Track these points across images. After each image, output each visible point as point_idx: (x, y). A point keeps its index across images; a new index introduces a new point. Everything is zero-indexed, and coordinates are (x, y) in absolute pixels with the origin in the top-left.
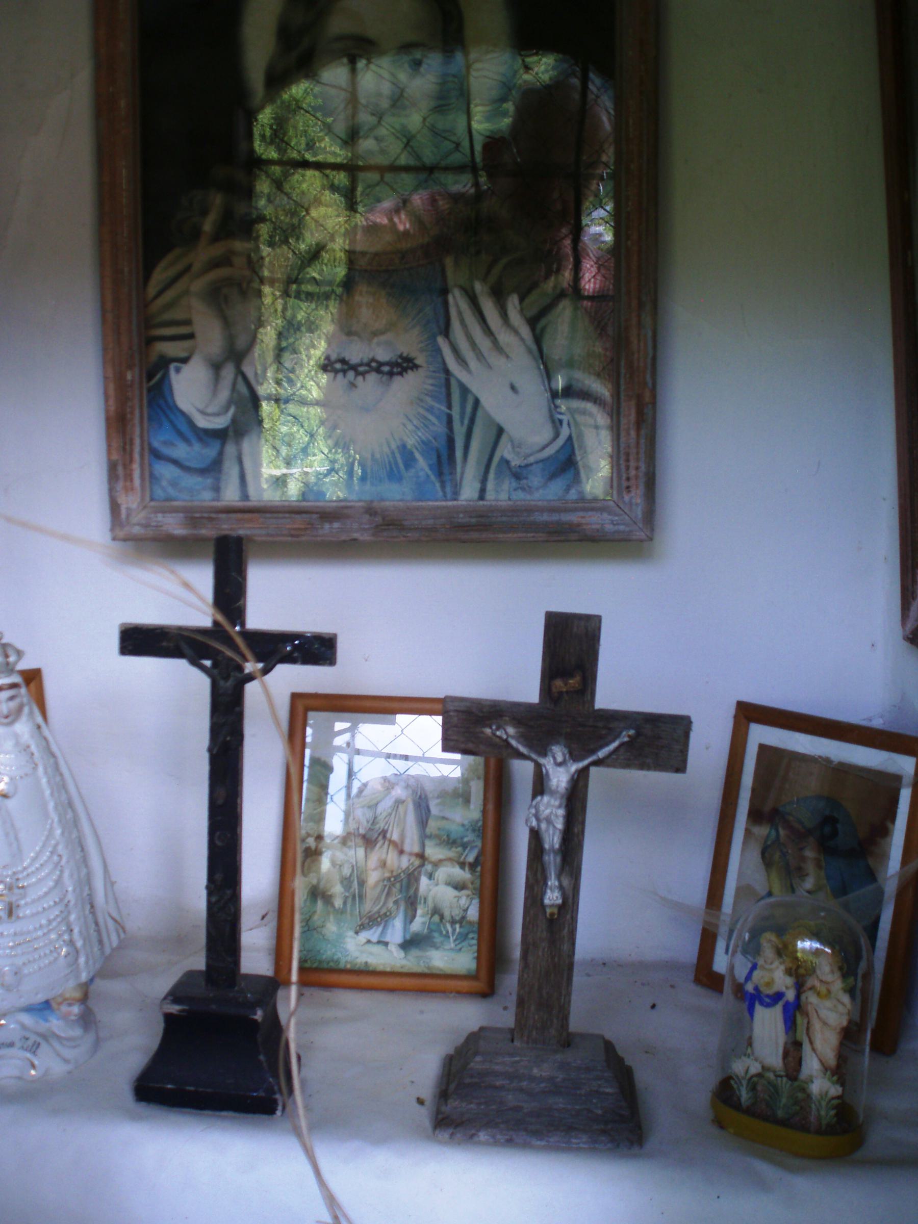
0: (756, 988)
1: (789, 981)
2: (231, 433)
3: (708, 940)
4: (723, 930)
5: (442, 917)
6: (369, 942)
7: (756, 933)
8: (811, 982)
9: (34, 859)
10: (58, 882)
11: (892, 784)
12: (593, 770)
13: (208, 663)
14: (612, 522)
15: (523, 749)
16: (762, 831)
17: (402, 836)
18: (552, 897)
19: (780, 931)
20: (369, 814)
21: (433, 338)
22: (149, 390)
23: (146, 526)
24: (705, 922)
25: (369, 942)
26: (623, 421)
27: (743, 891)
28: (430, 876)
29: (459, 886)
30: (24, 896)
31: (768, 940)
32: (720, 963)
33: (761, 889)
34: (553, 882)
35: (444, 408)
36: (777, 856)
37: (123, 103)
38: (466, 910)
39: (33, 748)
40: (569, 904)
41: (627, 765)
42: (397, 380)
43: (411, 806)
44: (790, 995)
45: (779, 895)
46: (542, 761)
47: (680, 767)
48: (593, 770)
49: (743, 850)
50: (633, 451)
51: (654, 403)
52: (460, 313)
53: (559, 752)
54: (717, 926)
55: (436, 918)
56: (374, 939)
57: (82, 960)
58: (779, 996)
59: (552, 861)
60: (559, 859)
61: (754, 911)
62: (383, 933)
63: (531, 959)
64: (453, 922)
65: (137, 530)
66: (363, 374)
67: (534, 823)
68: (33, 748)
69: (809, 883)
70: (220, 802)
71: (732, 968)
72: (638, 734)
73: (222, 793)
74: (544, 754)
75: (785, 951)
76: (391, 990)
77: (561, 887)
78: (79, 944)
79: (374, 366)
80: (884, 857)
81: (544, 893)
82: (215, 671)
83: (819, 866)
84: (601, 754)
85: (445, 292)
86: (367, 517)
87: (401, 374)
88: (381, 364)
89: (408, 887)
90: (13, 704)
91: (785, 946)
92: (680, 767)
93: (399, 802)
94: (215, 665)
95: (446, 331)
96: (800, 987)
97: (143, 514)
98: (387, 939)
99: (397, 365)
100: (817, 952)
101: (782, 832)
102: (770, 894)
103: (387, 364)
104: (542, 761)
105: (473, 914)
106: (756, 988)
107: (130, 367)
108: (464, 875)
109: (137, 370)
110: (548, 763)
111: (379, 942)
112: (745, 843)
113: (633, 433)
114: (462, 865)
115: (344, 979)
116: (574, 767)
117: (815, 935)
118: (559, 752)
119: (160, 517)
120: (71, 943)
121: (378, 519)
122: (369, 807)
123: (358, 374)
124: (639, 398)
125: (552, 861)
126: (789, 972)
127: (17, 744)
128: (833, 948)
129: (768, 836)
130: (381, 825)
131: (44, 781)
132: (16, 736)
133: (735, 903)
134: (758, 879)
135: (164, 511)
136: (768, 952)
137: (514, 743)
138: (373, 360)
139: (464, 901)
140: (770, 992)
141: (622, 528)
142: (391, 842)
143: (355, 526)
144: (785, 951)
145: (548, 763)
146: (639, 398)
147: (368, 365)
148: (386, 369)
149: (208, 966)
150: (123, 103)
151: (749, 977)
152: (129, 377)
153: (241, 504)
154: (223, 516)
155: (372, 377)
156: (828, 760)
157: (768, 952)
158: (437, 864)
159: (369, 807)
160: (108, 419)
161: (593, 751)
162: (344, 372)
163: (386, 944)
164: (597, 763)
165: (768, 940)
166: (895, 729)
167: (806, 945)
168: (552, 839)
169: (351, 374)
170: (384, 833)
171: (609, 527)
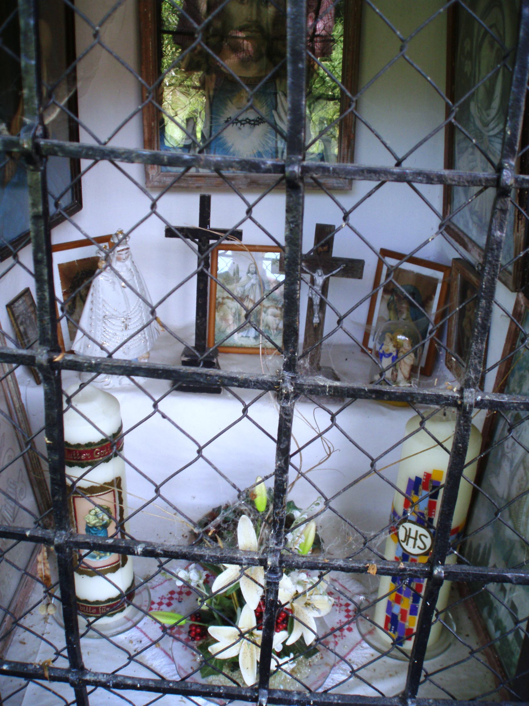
0: (383, 352)
1: (394, 349)
2: (192, 146)
3: (366, 336)
4: (372, 332)
5: (269, 328)
6: (242, 336)
7: (384, 333)
8: (401, 349)
9: (134, 309)
10: (141, 317)
11: (432, 282)
12: (331, 278)
13: (197, 240)
14: (337, 183)
15: (307, 271)
16: (387, 297)
17: (255, 298)
18: (316, 320)
19: (392, 333)
20: (242, 289)
21: (271, 111)
22: (160, 129)
23: (160, 182)
24: (366, 329)
25: (242, 336)
26: (342, 145)
27: (380, 319)
28: (265, 312)
29: (275, 316)
30: (130, 322)
31: (388, 336)
32: (371, 344)
33: (387, 318)
34: (316, 315)
35: (274, 138)
36: (393, 306)
37: (150, 16)
38: (278, 325)
39: (132, 270)
40: (321, 323)
41: (343, 276)
42: (257, 127)
43: (258, 286)
44: (394, 354)
45: (393, 321)
46: (314, 275)
47: (360, 277)
48: (331, 278)
49: (381, 304)
50: (346, 156)
51: (354, 139)
52: (281, 101)
53: (320, 272)
54: (370, 331)
55: (267, 328)
56: (244, 335)
57: (148, 344)
58: (390, 354)
59: (316, 308)
60: (319, 308)
61: (383, 326)
62: (248, 333)
63: (308, 341)
64: (273, 329)
65: (156, 184)
66: (244, 124)
67: (310, 295)
68: (132, 270)
69: (404, 316)
70: (201, 288)
71: (375, 347)
72: (347, 266)
73: (202, 286)
74: (315, 272)
75: (393, 339)
76: (250, 354)
77: (319, 317)
78: (147, 338)
79: (248, 121)
80: (431, 307)
81: (313, 319)
82: (200, 243)
83: (408, 310)
84: (334, 272)
85: (276, 94)
86: (244, 179)
87: (258, 125)
88: (250, 121)
89: (257, 316)
90: (127, 255)
91: (394, 338)
92: (360, 277)
93: (253, 285)
94: (200, 241)
95: (276, 108)
96: (398, 352)
97: (158, 177)
98: (249, 335)
99: (257, 121)
100: (405, 340)
101: (395, 298)
102: (390, 320)
103: (253, 120)
104: (314, 275)
105: (281, 326)
106: (383, 352)
107: (153, 121)
108: (278, 312)
109: (156, 122)
110: (316, 276)
111: (246, 337)
112: (381, 301)
113: (346, 150)
114: (277, 308)
115: (230, 350)
116: (325, 277)
117: (404, 334)
118: (320, 272)
119: (165, 178)
120: (145, 338)
121: (249, 180)
122: (242, 287)
123: (241, 124)
124: (349, 137)
125: (316, 308)
126: (394, 346)
127: (127, 269)
128: (408, 337)
129: (390, 299)
130: (246, 293)
131: (136, 281)
132: (127, 266)
133: (377, 323)
134: (386, 314)
135: (166, 176)
136: (388, 339)
137: (304, 268)
138: (247, 119)
139: (277, 322)
140: (388, 353)
141: (340, 185)
142: (250, 300)
143: (240, 183)
144: (393, 339)
145: (316, 276)
146: (349, 137)
147: (245, 120)
148: (253, 122)
149: (196, 344)
150: (150, 16)
151: (381, 348)
152: (153, 124)
153: (196, 174)
154: (189, 178)
155: (247, 126)
156: (413, 272)
157: (388, 339)
158: (268, 308)
159: (242, 287)
160: (144, 141)
161: (331, 272)
162: (237, 123)
163: (249, 337)
164: (332, 275)
165: (388, 336)
166: (438, 262)
167: (400, 337)
168: (317, 301)
169: (239, 124)
170: (247, 296)
171: (336, 185)
